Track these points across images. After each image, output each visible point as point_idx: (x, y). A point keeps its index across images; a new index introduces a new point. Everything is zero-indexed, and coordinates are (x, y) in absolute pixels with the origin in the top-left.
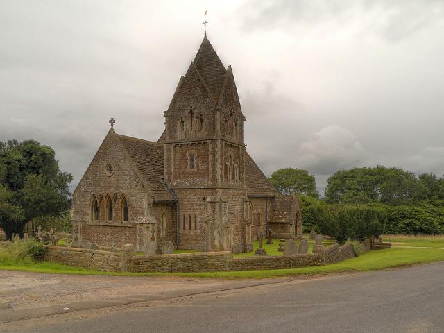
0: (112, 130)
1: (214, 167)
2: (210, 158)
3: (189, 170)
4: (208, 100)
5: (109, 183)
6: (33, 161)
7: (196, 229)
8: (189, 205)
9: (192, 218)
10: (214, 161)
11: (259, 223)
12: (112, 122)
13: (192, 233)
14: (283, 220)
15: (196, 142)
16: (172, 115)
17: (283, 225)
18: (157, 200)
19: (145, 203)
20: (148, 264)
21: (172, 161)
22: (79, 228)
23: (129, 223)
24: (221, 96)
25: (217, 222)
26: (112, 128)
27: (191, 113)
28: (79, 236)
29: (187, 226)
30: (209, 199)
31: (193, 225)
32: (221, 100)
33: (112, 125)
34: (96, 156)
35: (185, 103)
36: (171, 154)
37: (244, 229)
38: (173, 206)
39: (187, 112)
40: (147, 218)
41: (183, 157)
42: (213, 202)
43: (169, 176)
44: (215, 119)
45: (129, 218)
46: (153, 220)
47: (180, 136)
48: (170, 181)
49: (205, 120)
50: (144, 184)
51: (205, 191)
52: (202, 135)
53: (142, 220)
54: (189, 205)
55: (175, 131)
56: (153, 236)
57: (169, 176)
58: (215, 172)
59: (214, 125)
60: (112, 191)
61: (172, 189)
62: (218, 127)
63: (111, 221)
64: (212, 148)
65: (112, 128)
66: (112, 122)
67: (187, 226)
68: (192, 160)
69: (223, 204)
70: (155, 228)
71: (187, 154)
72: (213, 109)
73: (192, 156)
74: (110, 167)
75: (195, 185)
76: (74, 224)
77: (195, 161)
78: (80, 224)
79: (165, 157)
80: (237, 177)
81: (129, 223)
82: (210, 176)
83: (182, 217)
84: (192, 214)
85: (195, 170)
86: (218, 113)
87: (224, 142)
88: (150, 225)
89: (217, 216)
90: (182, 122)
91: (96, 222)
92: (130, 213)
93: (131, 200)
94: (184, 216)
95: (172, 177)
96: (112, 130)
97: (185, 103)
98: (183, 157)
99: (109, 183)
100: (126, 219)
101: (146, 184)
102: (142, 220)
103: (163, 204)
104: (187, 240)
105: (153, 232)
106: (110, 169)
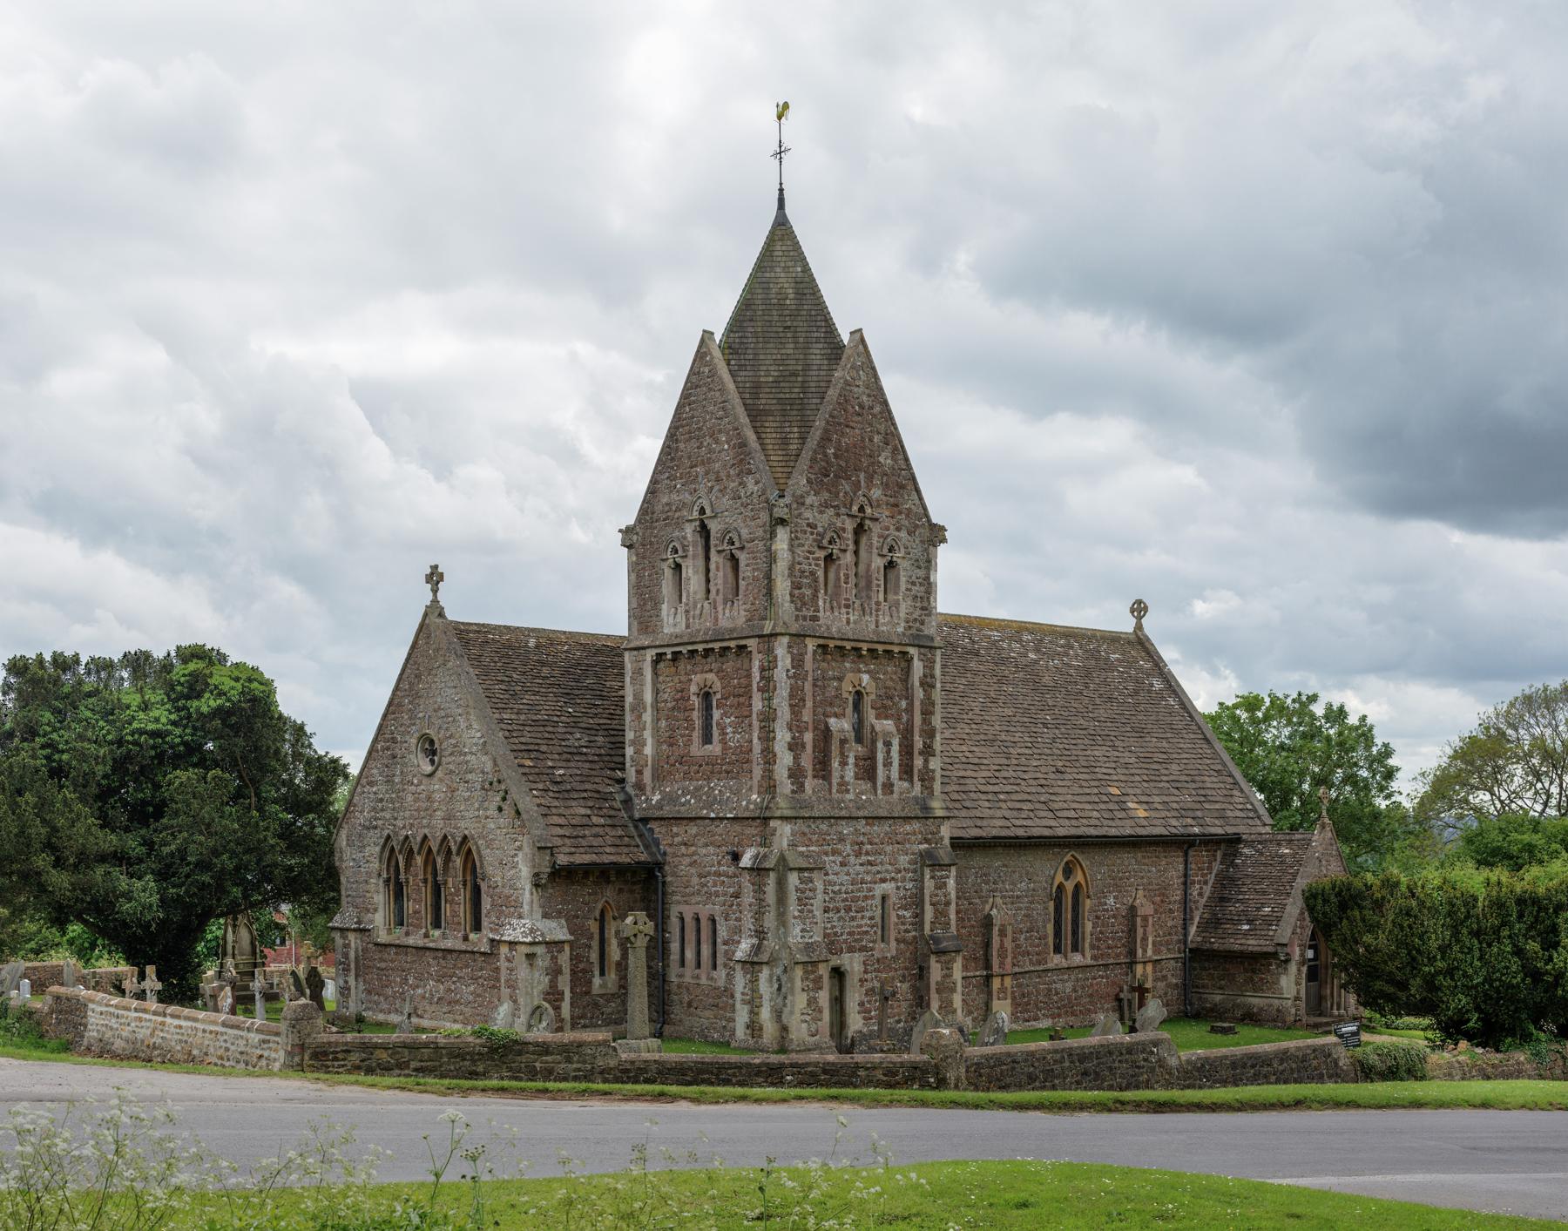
0: (435, 610)
1: (768, 737)
2: (758, 704)
3: (697, 749)
4: (750, 481)
5: (429, 798)
6: (224, 724)
7: (715, 967)
8: (695, 880)
9: (704, 924)
10: (768, 718)
11: (1132, 953)
12: (434, 577)
13: (704, 981)
14: (1253, 944)
15: (700, 647)
16: (645, 538)
17: (1260, 963)
18: (562, 860)
19: (525, 871)
20: (355, 1058)
21: (648, 717)
22: (352, 955)
23: (480, 941)
24: (804, 462)
25: (771, 943)
26: (435, 601)
27: (704, 531)
28: (352, 982)
29: (690, 954)
30: (746, 861)
31: (706, 951)
32: (799, 482)
33: (435, 591)
34: (390, 704)
35: (687, 497)
36: (640, 686)
37: (922, 973)
38: (645, 882)
39: (689, 530)
40: (526, 922)
41: (682, 696)
42: (758, 870)
43: (639, 772)
44: (772, 558)
45: (485, 923)
46: (558, 931)
47: (672, 623)
48: (640, 787)
49: (743, 557)
50: (521, 807)
51: (737, 827)
52: (733, 617)
53: (516, 930)
54: (695, 880)
55: (657, 604)
56: (553, 983)
57: (639, 772)
58: (769, 757)
59: (769, 577)
60: (436, 827)
61: (645, 820)
62: (782, 587)
63: (437, 933)
64: (762, 669)
65: (435, 601)
66: (434, 577)
67: (690, 954)
68: (708, 708)
69: (793, 879)
70: (564, 959)
71: (693, 688)
72: (764, 517)
73: (707, 696)
74: (432, 742)
75: (710, 807)
76: (337, 935)
77: (716, 714)
78: (351, 936)
79: (629, 699)
80: (889, 769)
81: (480, 941)
82: (758, 772)
83: (674, 922)
84: (705, 911)
85: (715, 748)
86: (782, 535)
87: (811, 644)
88: (540, 950)
89: (770, 921)
90: (678, 567)
91: (398, 936)
92: (486, 904)
93: (489, 860)
94: (682, 919)
95: (647, 774)
96: (435, 610)
97: (687, 497)
98: (682, 696)
99: (429, 798)
100: (477, 927)
101: (527, 803)
102: (516, 930)
103: (600, 874)
104: (690, 1005)
105: (555, 972)
106: (431, 751)
